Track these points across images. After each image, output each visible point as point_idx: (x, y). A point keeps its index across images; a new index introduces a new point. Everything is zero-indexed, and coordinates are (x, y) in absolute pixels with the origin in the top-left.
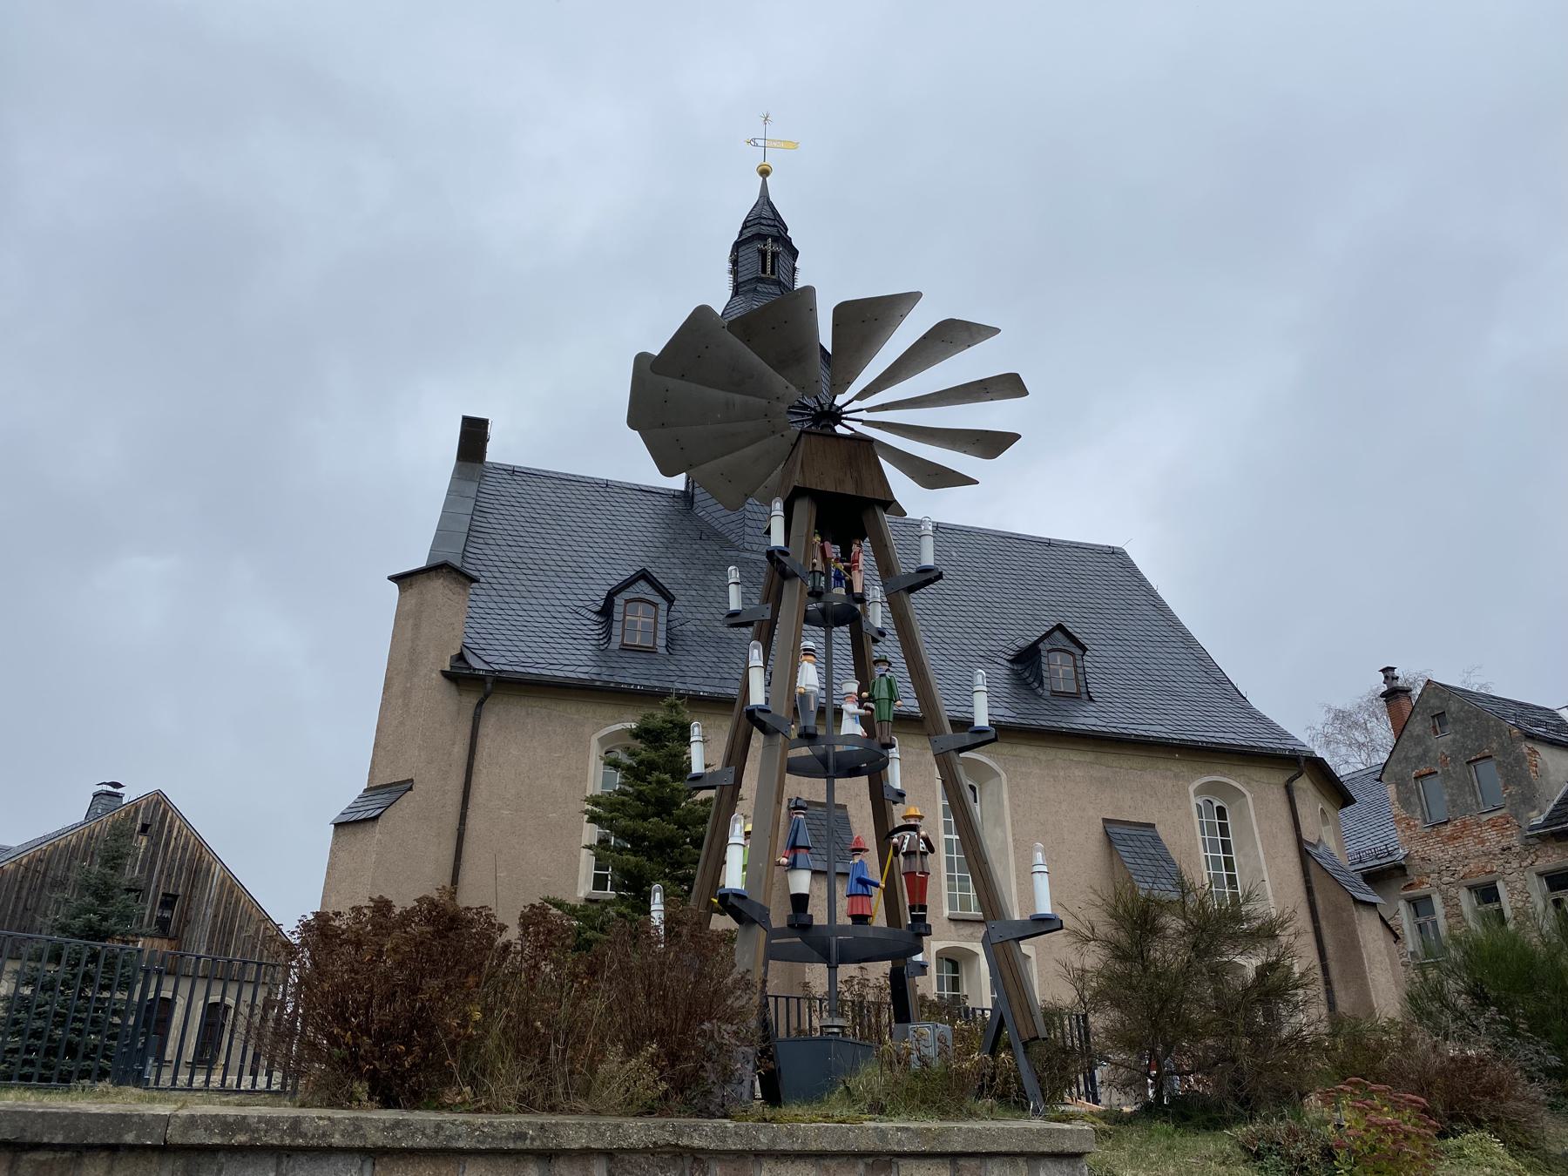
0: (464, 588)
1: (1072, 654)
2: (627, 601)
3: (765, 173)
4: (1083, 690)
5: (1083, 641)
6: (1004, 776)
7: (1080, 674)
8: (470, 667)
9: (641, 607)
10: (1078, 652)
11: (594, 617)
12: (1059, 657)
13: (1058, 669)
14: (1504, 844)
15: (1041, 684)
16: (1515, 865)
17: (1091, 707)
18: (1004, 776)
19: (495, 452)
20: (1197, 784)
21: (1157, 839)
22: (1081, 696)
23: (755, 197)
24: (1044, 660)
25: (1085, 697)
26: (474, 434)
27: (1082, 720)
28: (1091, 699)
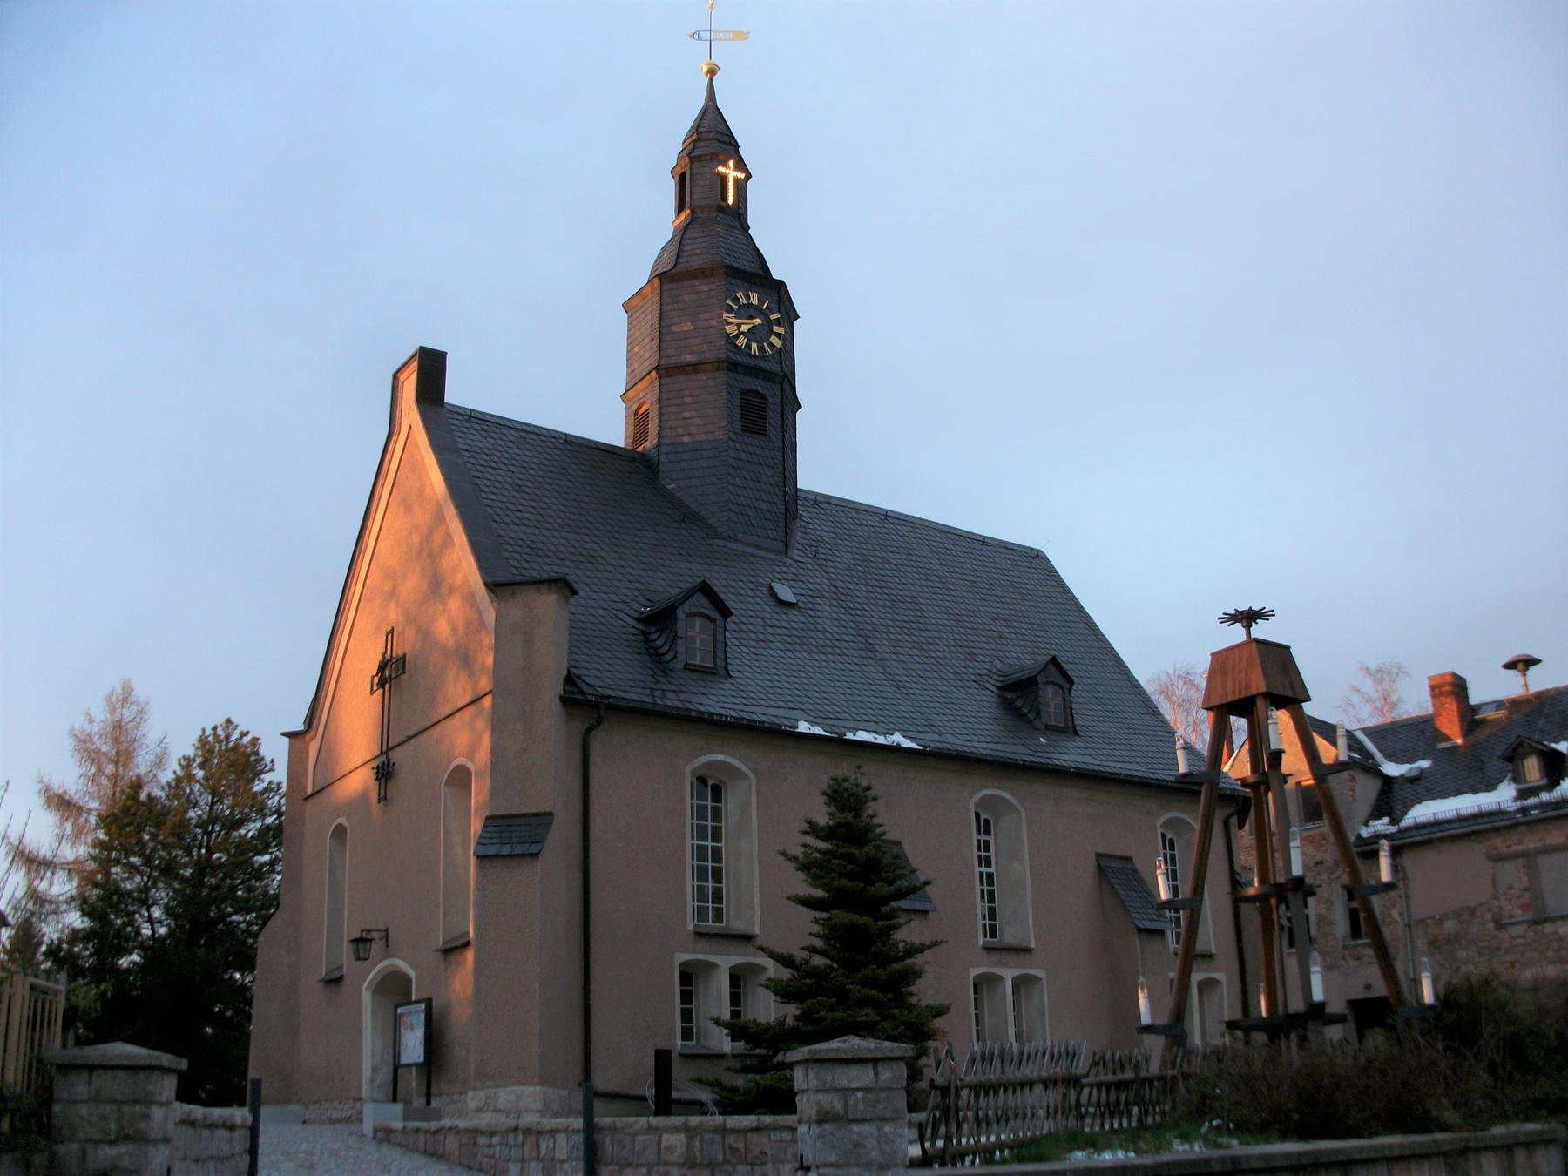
0: (566, 598)
1: (1061, 687)
2: (689, 615)
3: (712, 72)
4: (721, 663)
5: (730, 604)
6: (1023, 812)
7: (718, 647)
8: (582, 692)
9: (698, 622)
10: (1066, 685)
11: (632, 622)
12: (1050, 689)
13: (694, 634)
14: (1318, 859)
15: (1038, 714)
16: (1324, 877)
17: (1079, 742)
18: (1023, 812)
19: (455, 393)
20: (1163, 819)
21: (1135, 871)
22: (717, 671)
23: (699, 102)
24: (680, 624)
25: (722, 672)
26: (431, 366)
27: (1065, 757)
28: (1076, 734)
